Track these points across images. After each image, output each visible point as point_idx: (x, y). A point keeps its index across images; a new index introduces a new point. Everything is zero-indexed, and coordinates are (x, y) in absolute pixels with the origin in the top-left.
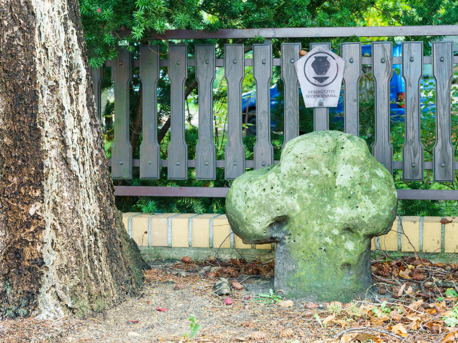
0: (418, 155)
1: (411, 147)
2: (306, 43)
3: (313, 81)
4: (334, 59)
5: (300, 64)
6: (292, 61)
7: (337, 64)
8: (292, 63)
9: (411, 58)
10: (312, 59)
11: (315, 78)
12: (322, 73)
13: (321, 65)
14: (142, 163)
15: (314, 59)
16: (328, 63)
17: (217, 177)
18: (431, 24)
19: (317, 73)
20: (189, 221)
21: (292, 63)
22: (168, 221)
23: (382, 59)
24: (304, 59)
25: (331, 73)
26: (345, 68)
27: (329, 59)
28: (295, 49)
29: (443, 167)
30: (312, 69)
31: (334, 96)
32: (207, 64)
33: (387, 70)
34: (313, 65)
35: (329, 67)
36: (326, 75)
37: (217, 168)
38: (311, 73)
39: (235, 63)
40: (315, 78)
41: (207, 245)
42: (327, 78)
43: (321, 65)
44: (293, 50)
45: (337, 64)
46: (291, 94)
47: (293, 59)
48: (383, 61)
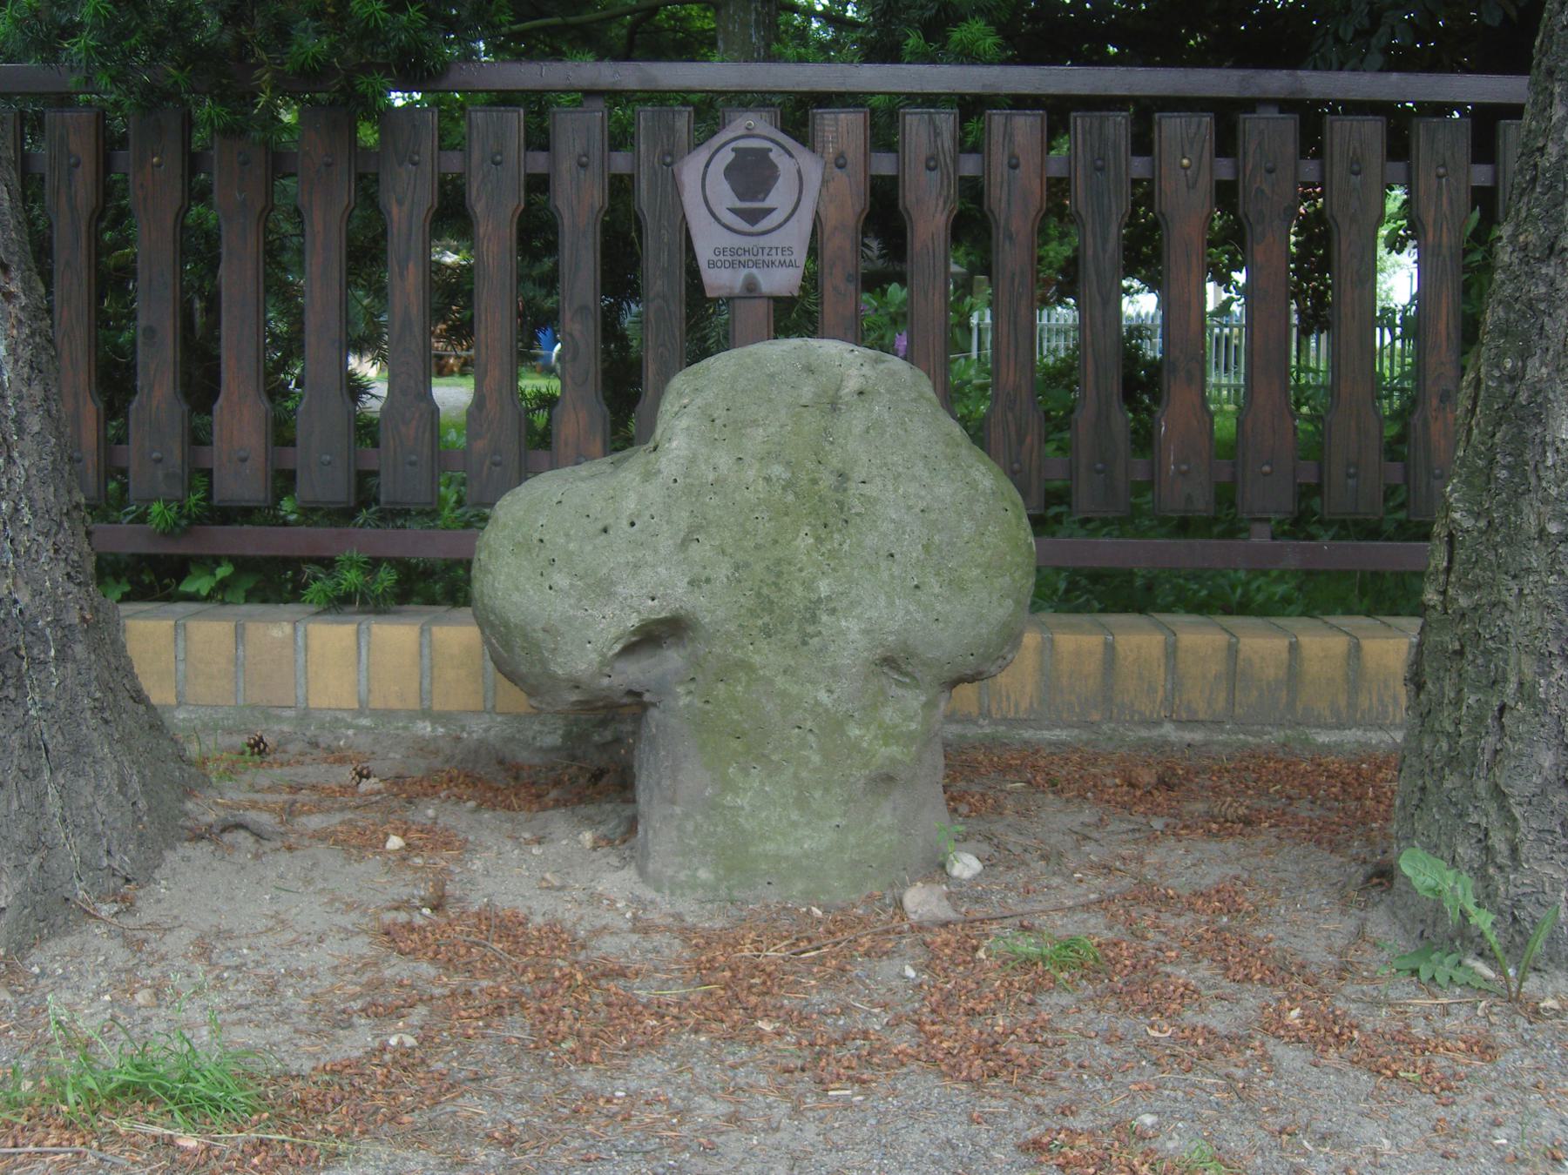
0: (1028, 440)
1: (1010, 416)
2: (709, 111)
3: (730, 219)
4: (791, 155)
5: (690, 170)
6: (668, 160)
7: (799, 172)
8: (668, 165)
9: (1012, 156)
10: (727, 156)
11: (734, 211)
12: (753, 199)
13: (751, 175)
14: (219, 455)
15: (732, 155)
16: (773, 167)
17: (119, 650)
18: (467, 565)
19: (741, 198)
20: (358, 632)
21: (668, 165)
22: (295, 629)
23: (928, 160)
24: (702, 155)
25: (779, 198)
26: (824, 182)
27: (776, 155)
28: (678, 124)
29: (1099, 472)
30: (725, 187)
31: (791, 265)
32: (414, 164)
33: (945, 193)
34: (729, 172)
35: (776, 178)
36: (767, 204)
37: (1319, 155)
38: (724, 195)
39: (497, 164)
40: (734, 211)
41: (413, 703)
42: (770, 211)
43: (751, 175)
44: (671, 130)
45: (799, 172)
46: (665, 257)
47: (670, 154)
48: (932, 164)
